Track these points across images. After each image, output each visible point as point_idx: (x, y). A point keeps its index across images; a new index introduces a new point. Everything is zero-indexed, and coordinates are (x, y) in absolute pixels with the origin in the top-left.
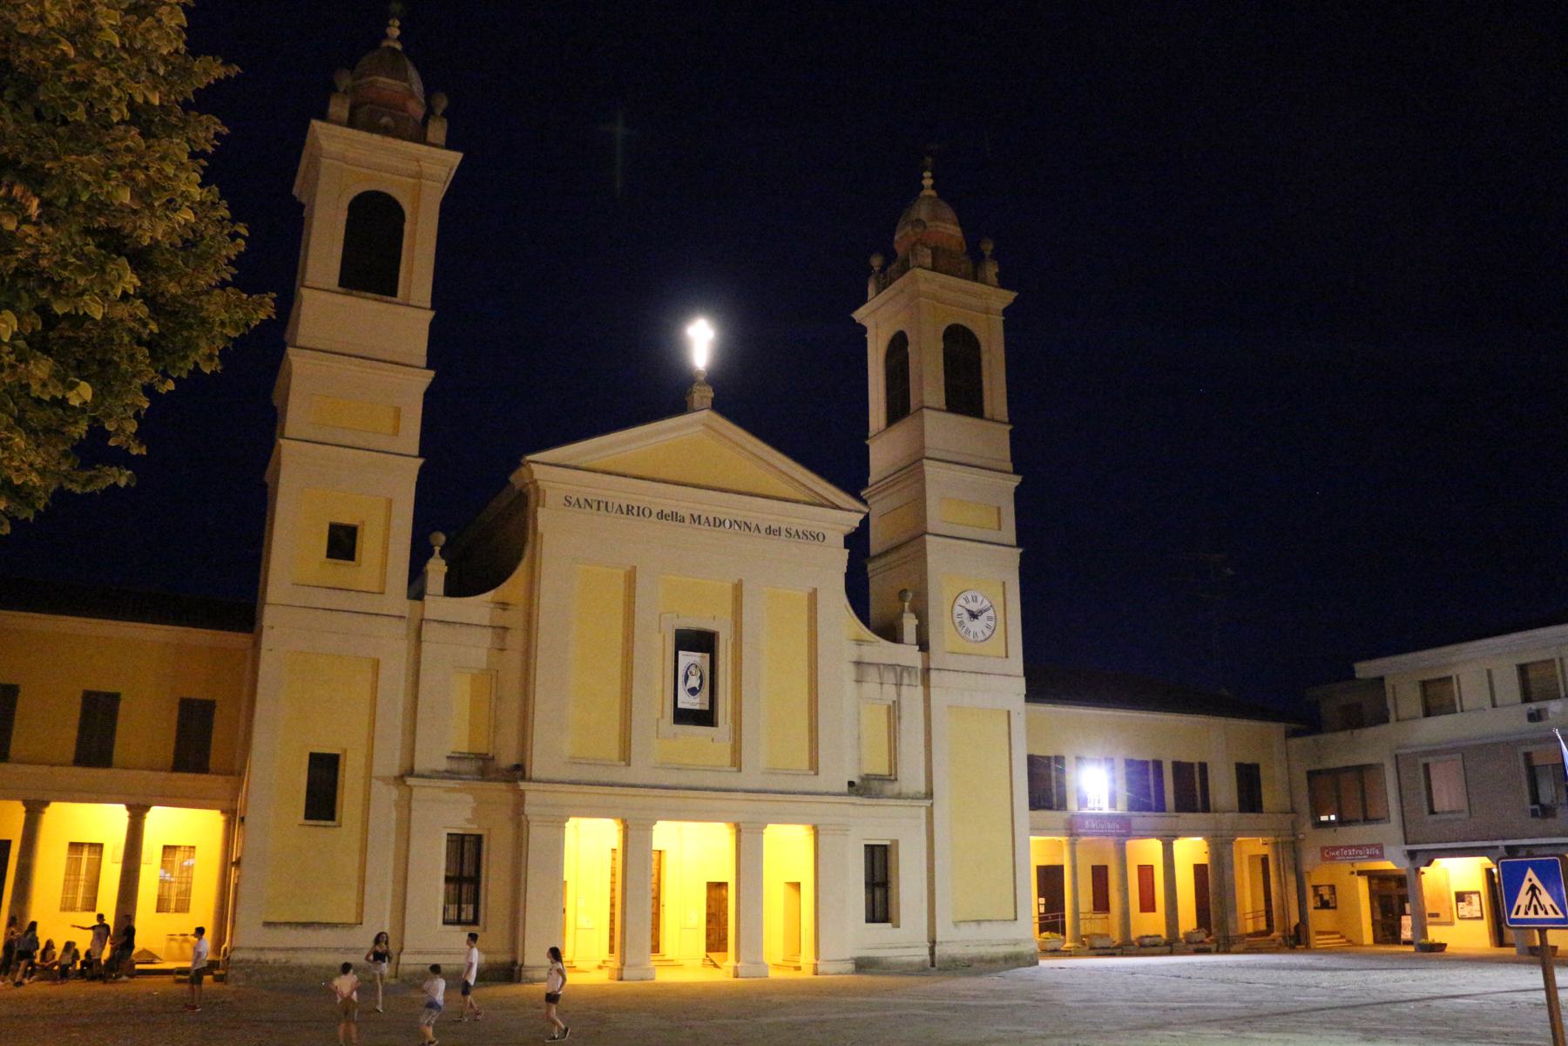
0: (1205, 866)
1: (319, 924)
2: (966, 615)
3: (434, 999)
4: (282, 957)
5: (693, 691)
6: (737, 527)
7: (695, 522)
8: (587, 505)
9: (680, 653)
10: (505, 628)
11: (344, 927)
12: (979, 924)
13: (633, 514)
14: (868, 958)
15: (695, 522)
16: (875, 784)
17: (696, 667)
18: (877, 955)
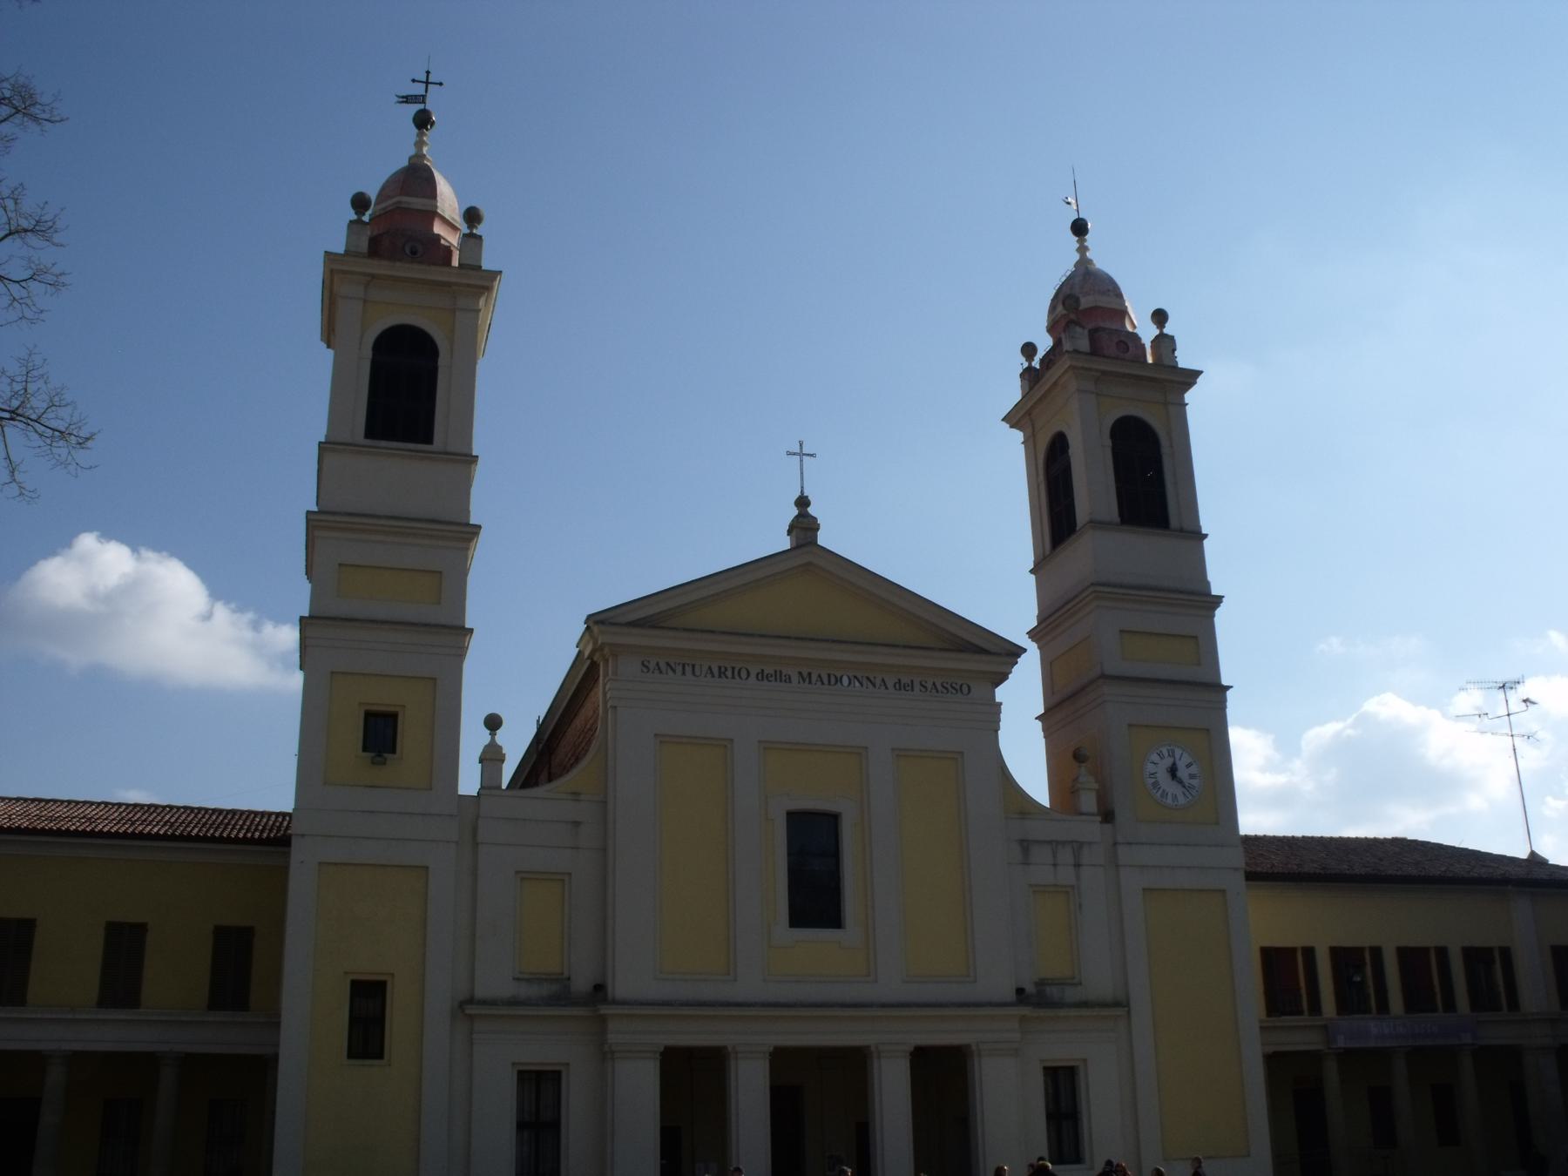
6: (857, 684)
13: (727, 677)
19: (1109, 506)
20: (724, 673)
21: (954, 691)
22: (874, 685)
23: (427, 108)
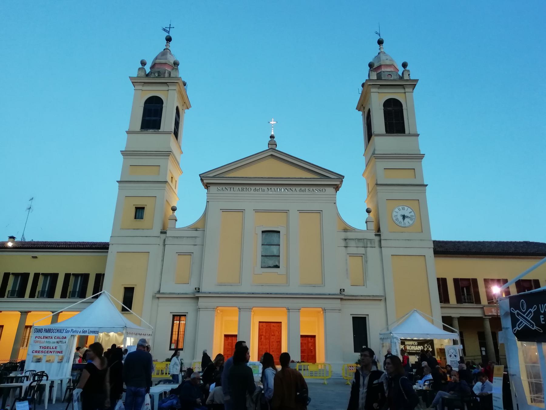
3: (538, 346)
6: (286, 191)
7: (269, 190)
8: (226, 189)
13: (244, 191)
19: (383, 130)
20: (243, 190)
21: (320, 191)
22: (292, 191)
23: (170, 35)
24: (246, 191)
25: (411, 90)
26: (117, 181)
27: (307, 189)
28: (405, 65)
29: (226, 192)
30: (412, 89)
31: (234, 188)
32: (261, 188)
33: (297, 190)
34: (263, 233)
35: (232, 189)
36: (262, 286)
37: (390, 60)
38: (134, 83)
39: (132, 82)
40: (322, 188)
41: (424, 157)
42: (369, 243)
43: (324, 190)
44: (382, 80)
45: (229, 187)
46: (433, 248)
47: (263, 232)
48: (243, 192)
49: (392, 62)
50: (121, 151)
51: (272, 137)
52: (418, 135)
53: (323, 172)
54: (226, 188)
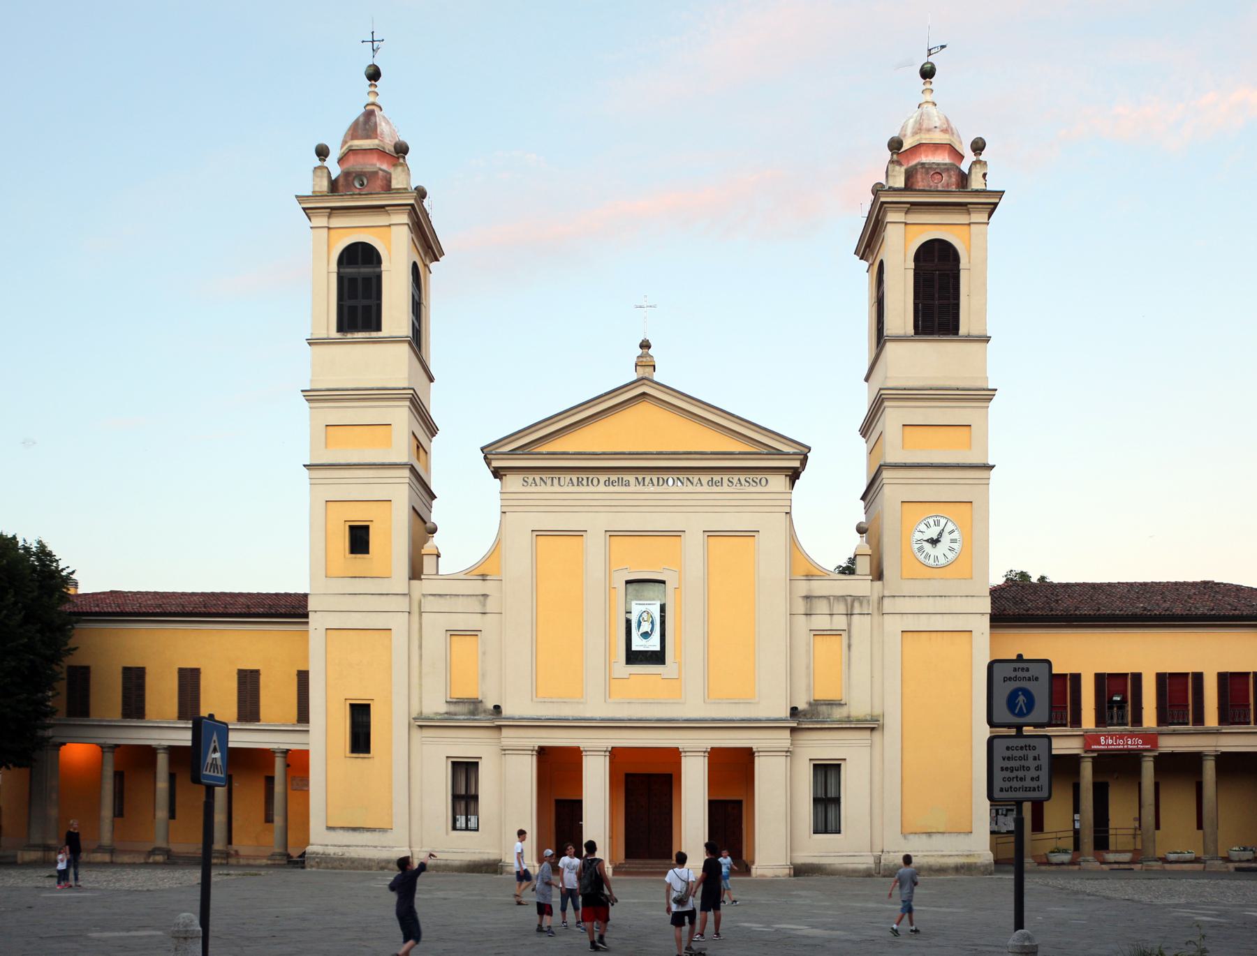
0: (1141, 726)
1: (363, 829)
2: (927, 546)
4: (339, 851)
5: (646, 635)
6: (679, 484)
9: (658, 648)
10: (485, 596)
11: (380, 831)
12: (930, 836)
13: (583, 485)
14: (812, 864)
15: (639, 484)
16: (823, 709)
17: (648, 613)
18: (821, 862)
21: (754, 484)
22: (692, 484)
24: (588, 485)
25: (982, 217)
26: (304, 466)
27: (725, 478)
28: (978, 146)
29: (542, 488)
30: (987, 216)
31: (559, 478)
32: (620, 476)
33: (702, 482)
34: (628, 585)
35: (556, 481)
36: (629, 703)
37: (945, 131)
38: (307, 211)
39: (303, 208)
40: (759, 477)
41: (994, 395)
42: (856, 605)
43: (764, 482)
44: (916, 190)
45: (549, 476)
46: (991, 614)
47: (628, 582)
48: (581, 489)
49: (947, 136)
50: (302, 391)
51: (645, 345)
52: (986, 339)
53: (763, 437)
54: (541, 478)
